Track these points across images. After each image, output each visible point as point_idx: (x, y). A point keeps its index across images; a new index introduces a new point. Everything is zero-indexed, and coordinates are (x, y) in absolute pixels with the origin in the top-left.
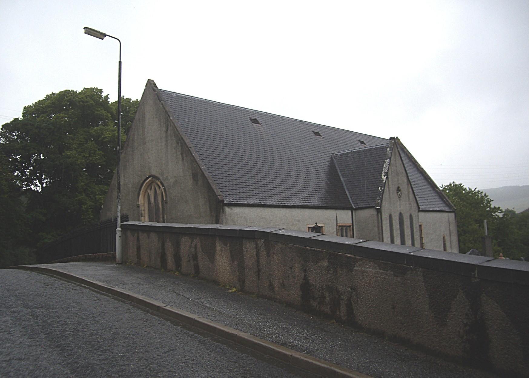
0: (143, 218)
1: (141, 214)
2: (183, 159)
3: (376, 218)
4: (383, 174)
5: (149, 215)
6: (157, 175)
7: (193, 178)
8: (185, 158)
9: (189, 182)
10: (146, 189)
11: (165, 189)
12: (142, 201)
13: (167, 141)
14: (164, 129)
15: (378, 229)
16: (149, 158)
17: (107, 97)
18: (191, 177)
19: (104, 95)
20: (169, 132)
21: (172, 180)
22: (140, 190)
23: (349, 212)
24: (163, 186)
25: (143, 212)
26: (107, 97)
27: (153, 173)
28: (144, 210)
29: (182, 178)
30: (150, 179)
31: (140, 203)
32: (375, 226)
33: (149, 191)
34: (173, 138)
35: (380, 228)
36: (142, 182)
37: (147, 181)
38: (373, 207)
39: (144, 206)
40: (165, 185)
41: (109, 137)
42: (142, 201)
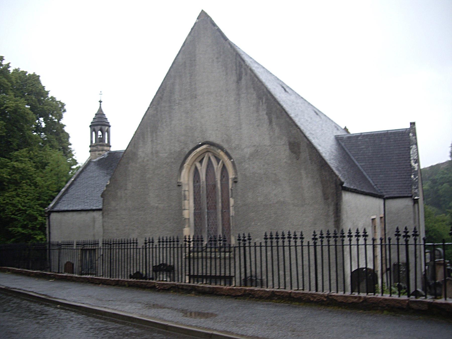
0: (186, 202)
1: (185, 196)
2: (271, 122)
3: (411, 209)
4: (412, 161)
5: (195, 199)
6: (222, 144)
7: (290, 149)
8: (274, 120)
9: (283, 152)
10: (195, 161)
11: (233, 163)
12: (186, 179)
13: (238, 95)
14: (234, 78)
15: (415, 222)
16: (202, 117)
17: (8, 66)
18: (287, 147)
19: (4, 63)
20: (243, 82)
21: (248, 151)
22: (183, 163)
23: (381, 202)
24: (230, 158)
25: (187, 193)
26: (8, 66)
27: (212, 139)
28: (188, 191)
29: (269, 148)
30: (204, 146)
31: (182, 180)
32: (410, 218)
33: (198, 165)
34: (252, 90)
35: (417, 220)
36: (187, 151)
37: (198, 150)
38: (411, 197)
39: (188, 184)
40: (233, 156)
41: (13, 106)
42: (186, 177)
